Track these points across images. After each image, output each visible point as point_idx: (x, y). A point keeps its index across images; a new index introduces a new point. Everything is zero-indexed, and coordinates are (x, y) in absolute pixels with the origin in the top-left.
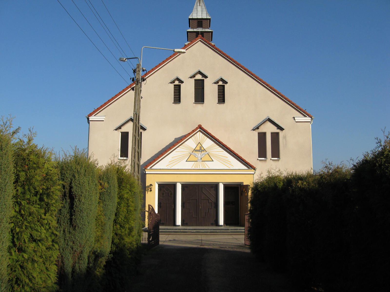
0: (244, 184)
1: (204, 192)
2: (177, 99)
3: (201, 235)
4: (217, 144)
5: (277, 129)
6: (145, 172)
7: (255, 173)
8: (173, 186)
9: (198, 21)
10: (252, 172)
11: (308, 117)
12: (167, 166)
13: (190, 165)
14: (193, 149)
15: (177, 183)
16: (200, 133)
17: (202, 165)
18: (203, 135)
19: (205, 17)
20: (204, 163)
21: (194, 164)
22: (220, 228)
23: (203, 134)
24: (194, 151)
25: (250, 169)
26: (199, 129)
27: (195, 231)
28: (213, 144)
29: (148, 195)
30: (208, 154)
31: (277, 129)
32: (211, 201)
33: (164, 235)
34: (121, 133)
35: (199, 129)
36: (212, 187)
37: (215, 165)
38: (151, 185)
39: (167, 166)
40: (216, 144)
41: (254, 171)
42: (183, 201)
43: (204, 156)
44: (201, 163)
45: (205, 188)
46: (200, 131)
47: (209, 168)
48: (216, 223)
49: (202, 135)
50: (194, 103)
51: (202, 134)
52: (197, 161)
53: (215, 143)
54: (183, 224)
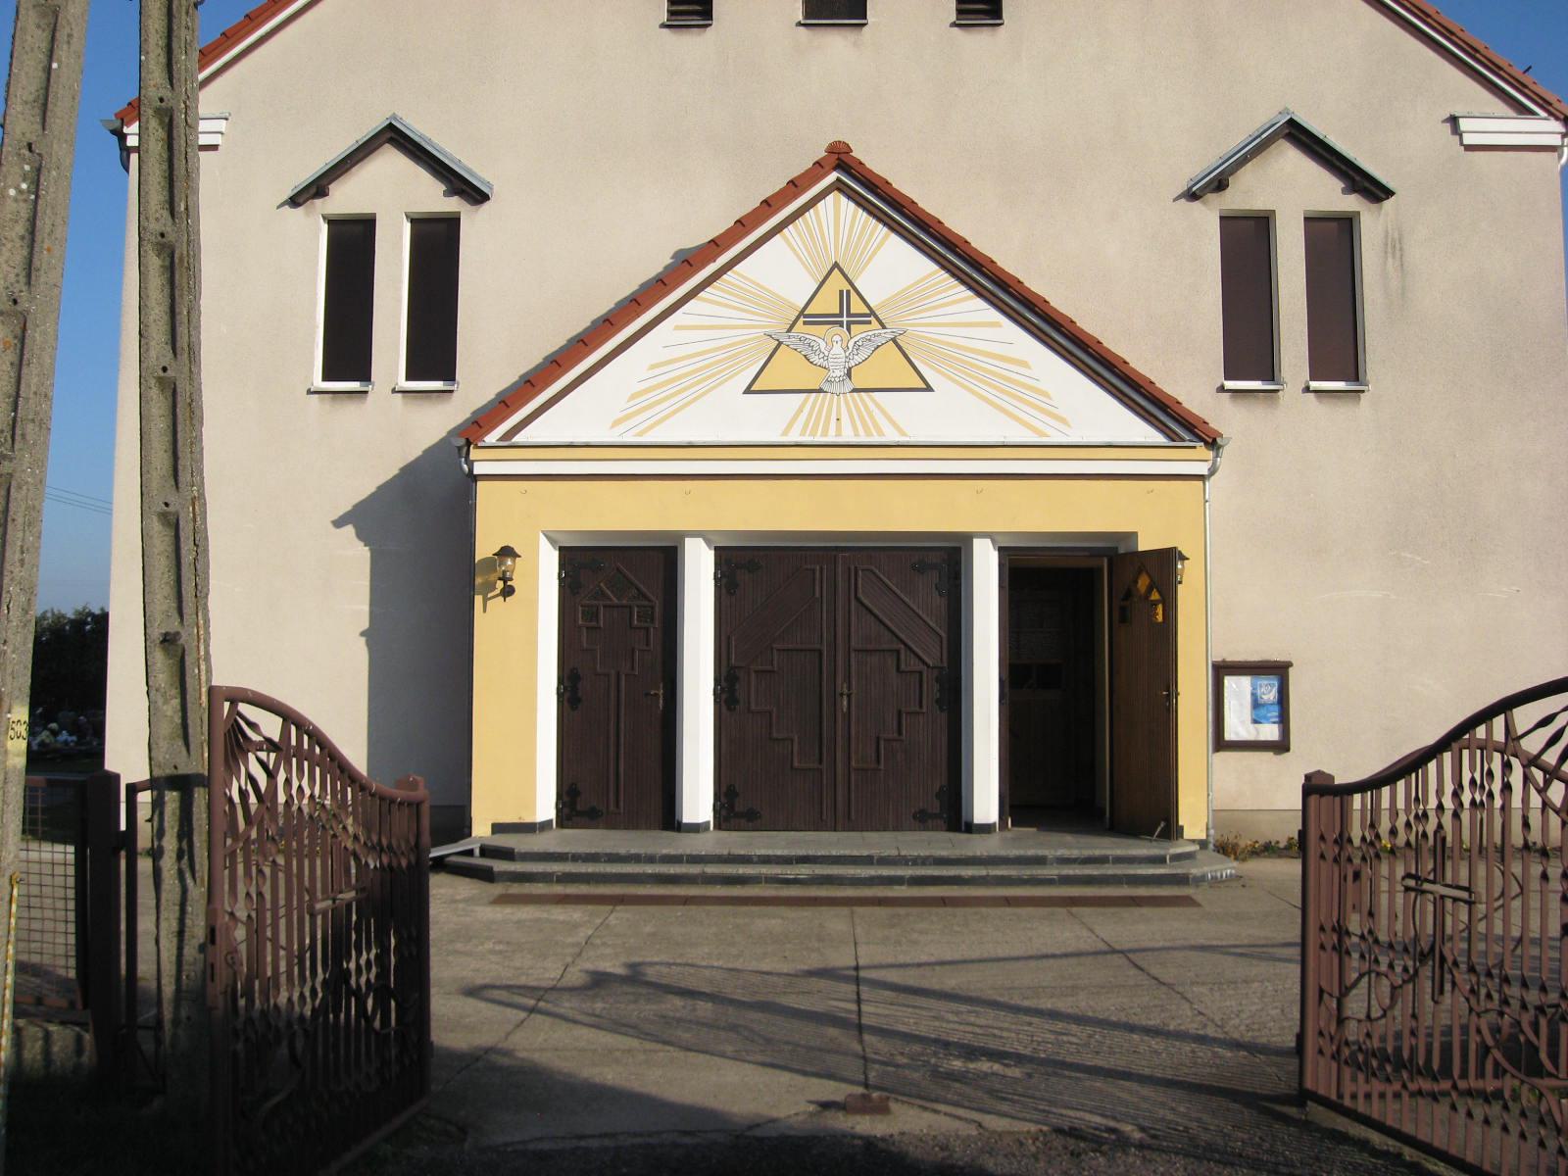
0: (1144, 545)
1: (866, 602)
3: (845, 911)
4: (953, 275)
5: (1347, 191)
6: (470, 464)
7: (1213, 471)
11: (1543, 114)
12: (617, 423)
14: (792, 306)
15: (688, 541)
16: (843, 200)
17: (858, 423)
18: (862, 215)
20: (870, 404)
21: (801, 410)
22: (979, 846)
23: (858, 204)
24: (802, 319)
25: (1183, 440)
26: (833, 176)
27: (804, 871)
28: (929, 276)
29: (490, 620)
30: (894, 340)
31: (1345, 191)
32: (913, 660)
33: (576, 914)
34: (325, 227)
35: (833, 176)
36: (921, 568)
38: (507, 552)
39: (617, 423)
40: (947, 275)
41: (1210, 454)
42: (729, 659)
43: (864, 353)
44: (847, 404)
45: (872, 571)
46: (839, 190)
47: (904, 434)
48: (953, 812)
49: (854, 217)
50: (799, 24)
51: (852, 205)
52: (820, 391)
53: (943, 267)
54: (727, 819)
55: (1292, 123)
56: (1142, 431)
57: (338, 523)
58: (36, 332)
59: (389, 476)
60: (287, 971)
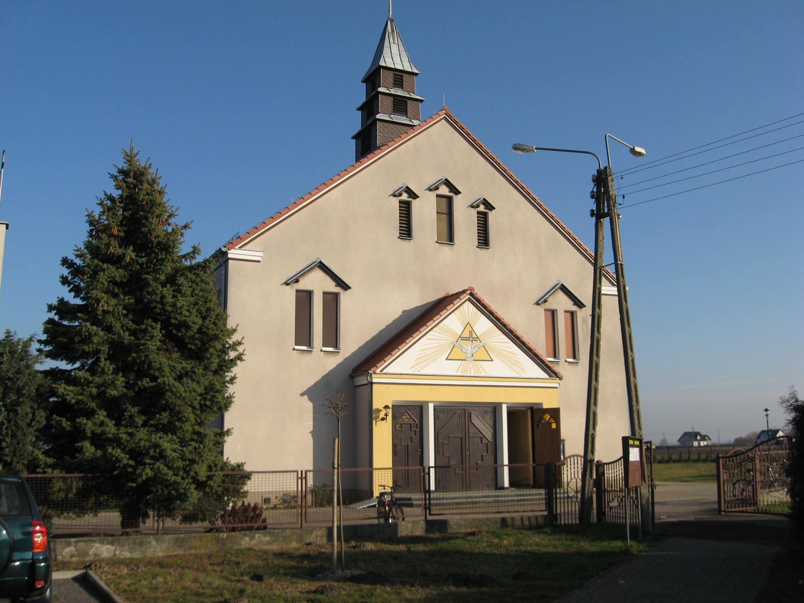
2: (406, 231)
4: (498, 328)
8: (419, 409)
9: (395, 74)
10: (554, 383)
12: (412, 368)
13: (452, 368)
16: (470, 303)
19: (408, 68)
21: (461, 365)
30: (483, 346)
31: (336, 286)
35: (468, 296)
37: (492, 369)
39: (412, 368)
55: (320, 262)
56: (544, 375)
57: (302, 395)
58: (130, 320)
59: (317, 380)
60: (406, 544)
